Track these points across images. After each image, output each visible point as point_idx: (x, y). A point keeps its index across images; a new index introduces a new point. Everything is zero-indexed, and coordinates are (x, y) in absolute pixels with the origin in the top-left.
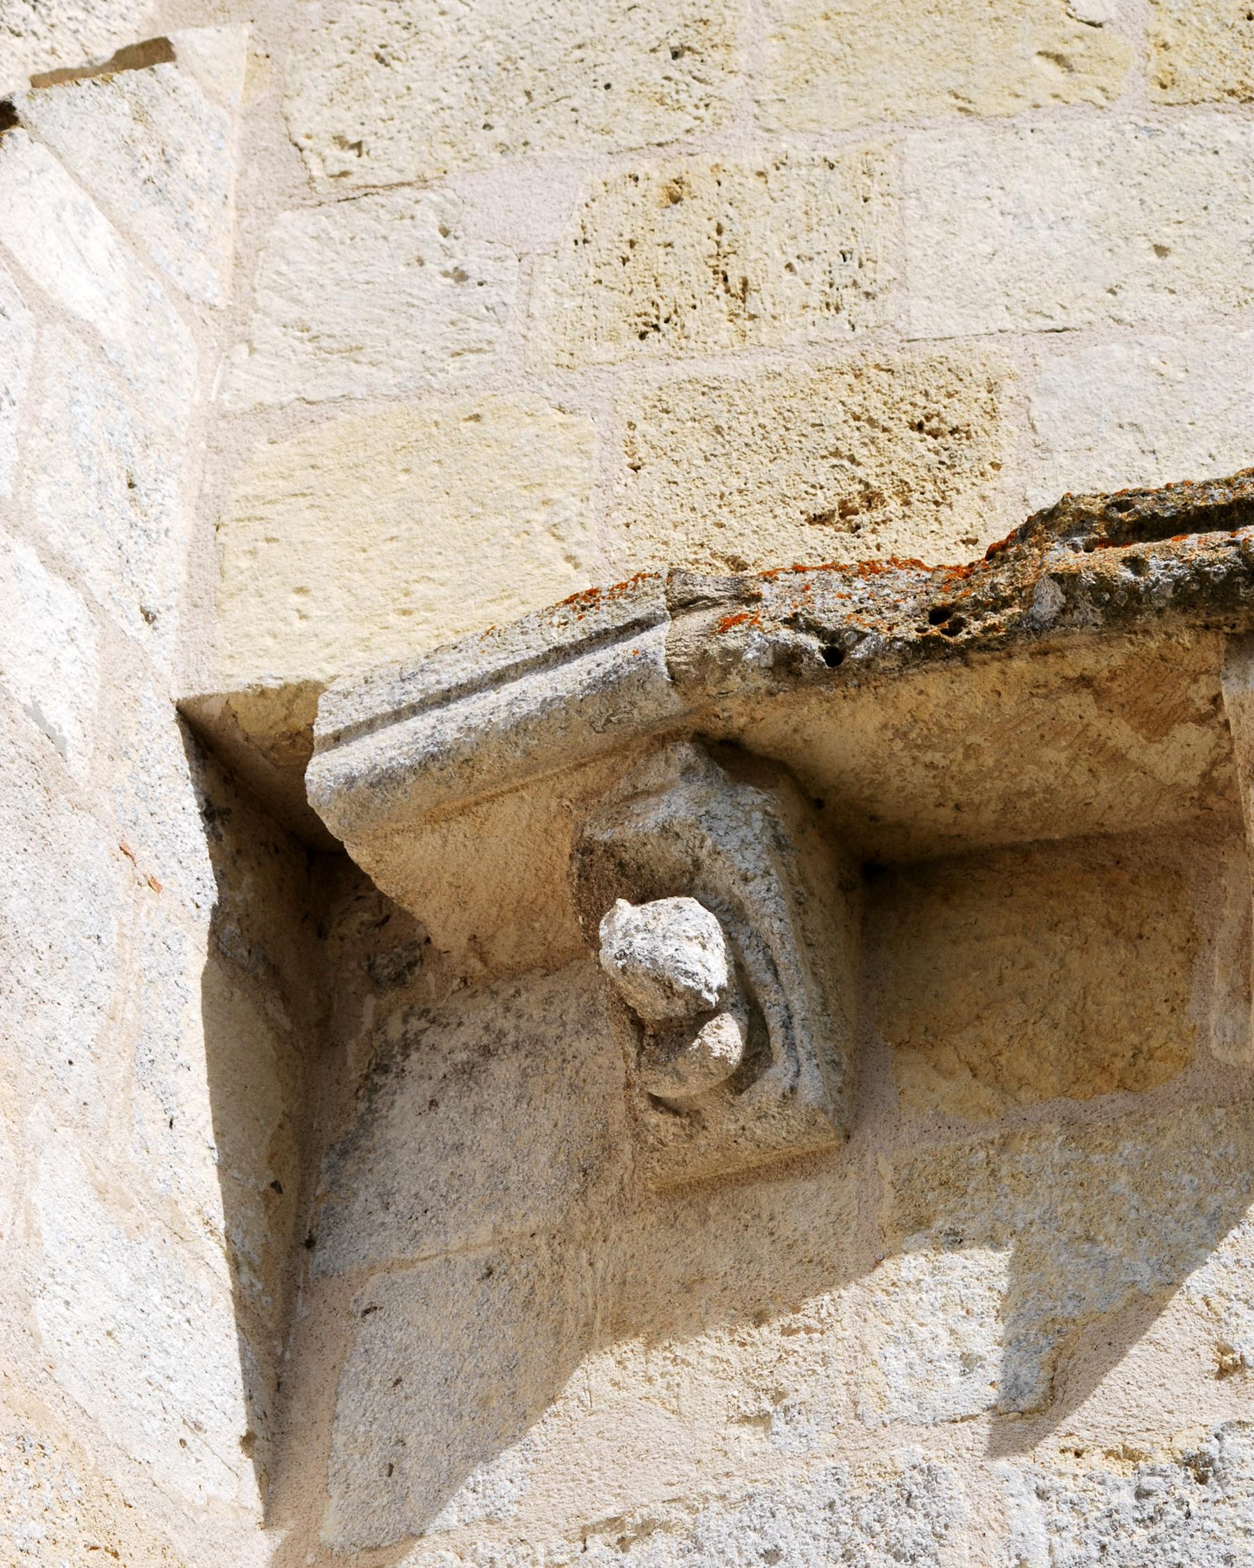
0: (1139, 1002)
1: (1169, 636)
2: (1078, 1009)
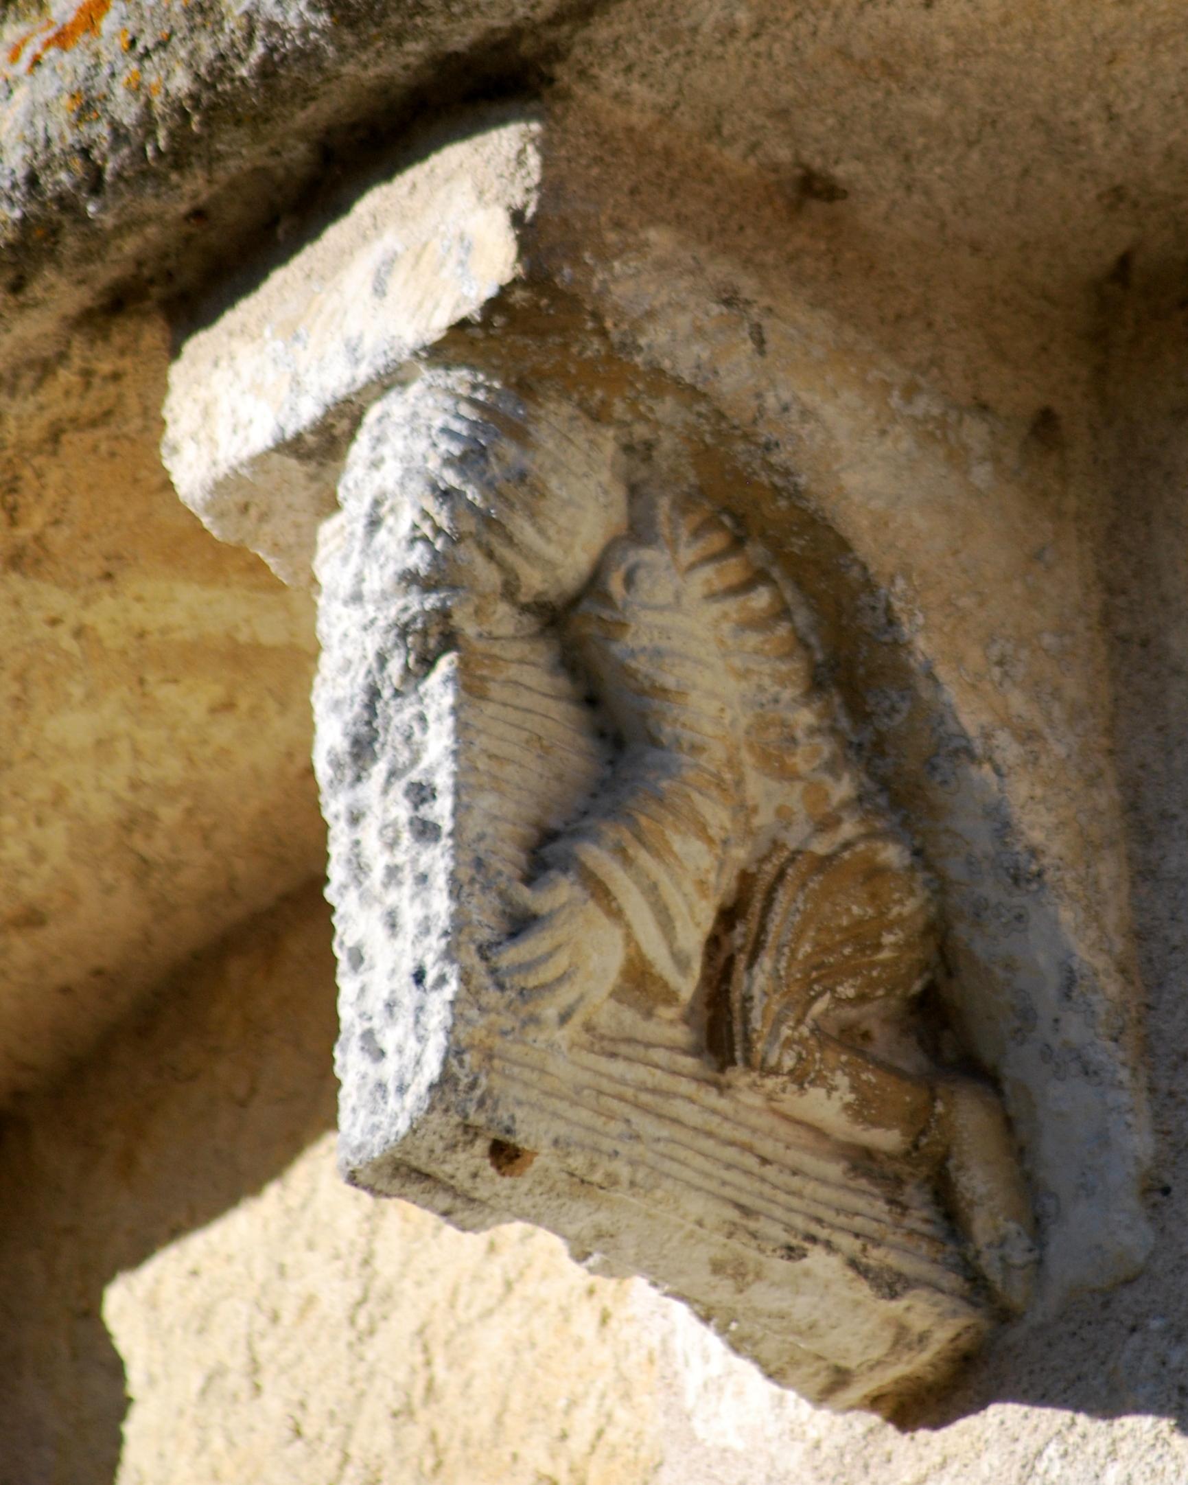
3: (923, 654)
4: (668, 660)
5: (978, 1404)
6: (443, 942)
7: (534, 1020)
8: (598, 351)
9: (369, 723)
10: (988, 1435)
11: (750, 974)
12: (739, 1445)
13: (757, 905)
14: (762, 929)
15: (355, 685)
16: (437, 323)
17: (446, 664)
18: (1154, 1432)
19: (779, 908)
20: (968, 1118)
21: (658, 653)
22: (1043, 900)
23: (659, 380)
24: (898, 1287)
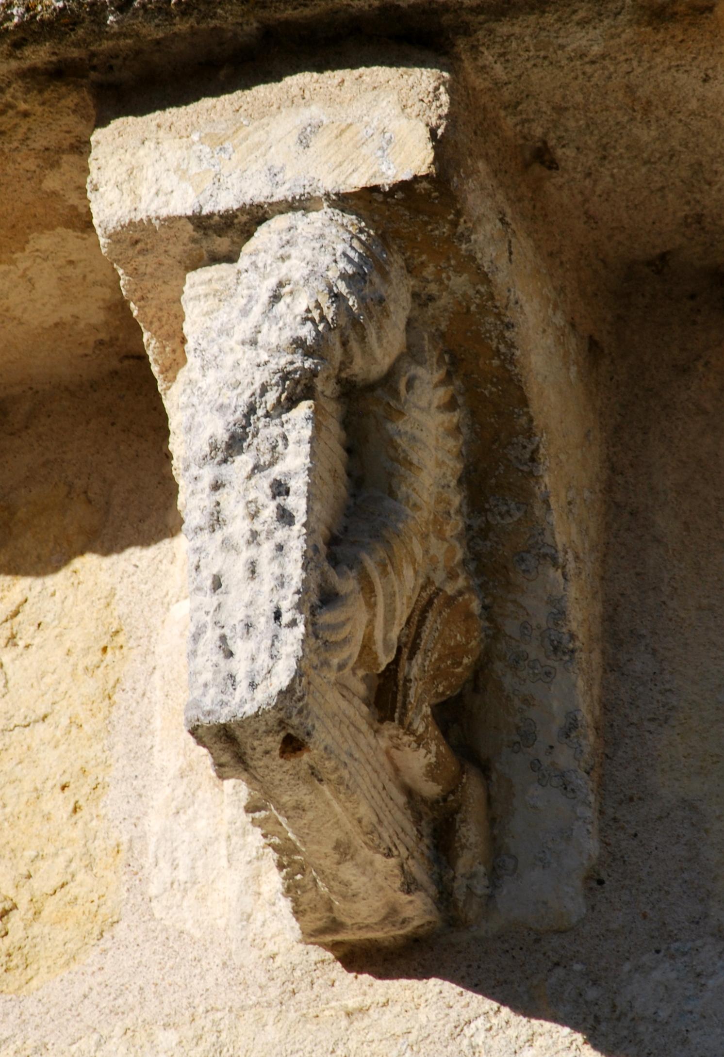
3: (546, 486)
4: (418, 444)
5: (423, 974)
6: (297, 597)
7: (326, 663)
8: (444, 233)
9: (244, 428)
10: (429, 996)
11: (410, 664)
15: (240, 400)
16: (358, 181)
17: (304, 408)
18: (570, 1039)
19: (428, 623)
20: (473, 789)
21: (414, 438)
22: (571, 669)
23: (469, 263)
24: (413, 887)
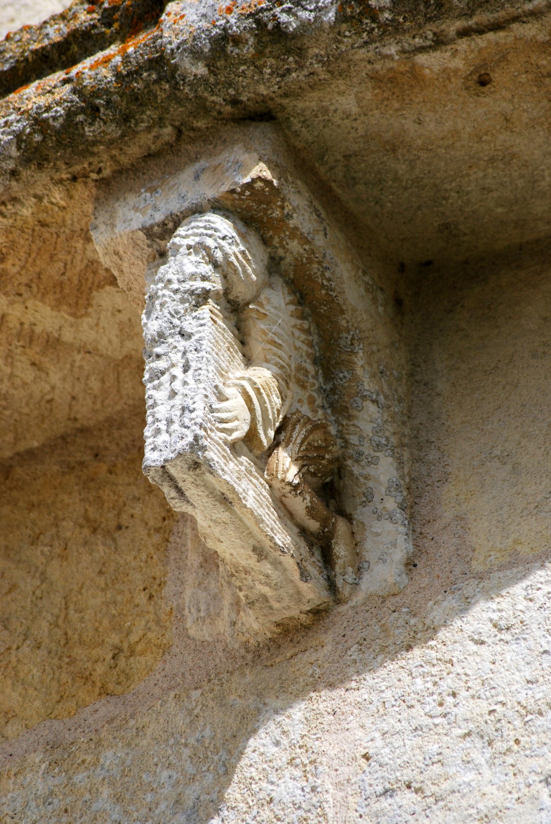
0: (119, 598)
1: (39, 198)
2: (60, 622)
12: (210, 640)
13: (290, 428)
14: (291, 436)
20: (342, 526)
